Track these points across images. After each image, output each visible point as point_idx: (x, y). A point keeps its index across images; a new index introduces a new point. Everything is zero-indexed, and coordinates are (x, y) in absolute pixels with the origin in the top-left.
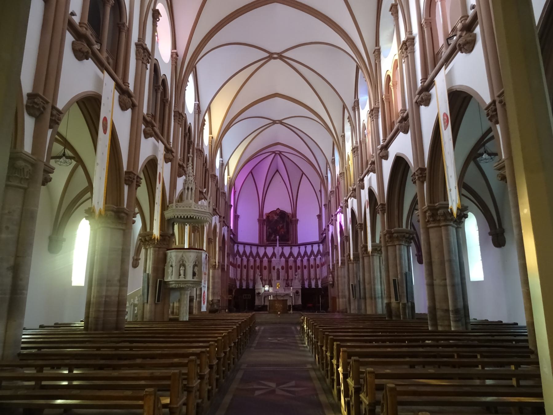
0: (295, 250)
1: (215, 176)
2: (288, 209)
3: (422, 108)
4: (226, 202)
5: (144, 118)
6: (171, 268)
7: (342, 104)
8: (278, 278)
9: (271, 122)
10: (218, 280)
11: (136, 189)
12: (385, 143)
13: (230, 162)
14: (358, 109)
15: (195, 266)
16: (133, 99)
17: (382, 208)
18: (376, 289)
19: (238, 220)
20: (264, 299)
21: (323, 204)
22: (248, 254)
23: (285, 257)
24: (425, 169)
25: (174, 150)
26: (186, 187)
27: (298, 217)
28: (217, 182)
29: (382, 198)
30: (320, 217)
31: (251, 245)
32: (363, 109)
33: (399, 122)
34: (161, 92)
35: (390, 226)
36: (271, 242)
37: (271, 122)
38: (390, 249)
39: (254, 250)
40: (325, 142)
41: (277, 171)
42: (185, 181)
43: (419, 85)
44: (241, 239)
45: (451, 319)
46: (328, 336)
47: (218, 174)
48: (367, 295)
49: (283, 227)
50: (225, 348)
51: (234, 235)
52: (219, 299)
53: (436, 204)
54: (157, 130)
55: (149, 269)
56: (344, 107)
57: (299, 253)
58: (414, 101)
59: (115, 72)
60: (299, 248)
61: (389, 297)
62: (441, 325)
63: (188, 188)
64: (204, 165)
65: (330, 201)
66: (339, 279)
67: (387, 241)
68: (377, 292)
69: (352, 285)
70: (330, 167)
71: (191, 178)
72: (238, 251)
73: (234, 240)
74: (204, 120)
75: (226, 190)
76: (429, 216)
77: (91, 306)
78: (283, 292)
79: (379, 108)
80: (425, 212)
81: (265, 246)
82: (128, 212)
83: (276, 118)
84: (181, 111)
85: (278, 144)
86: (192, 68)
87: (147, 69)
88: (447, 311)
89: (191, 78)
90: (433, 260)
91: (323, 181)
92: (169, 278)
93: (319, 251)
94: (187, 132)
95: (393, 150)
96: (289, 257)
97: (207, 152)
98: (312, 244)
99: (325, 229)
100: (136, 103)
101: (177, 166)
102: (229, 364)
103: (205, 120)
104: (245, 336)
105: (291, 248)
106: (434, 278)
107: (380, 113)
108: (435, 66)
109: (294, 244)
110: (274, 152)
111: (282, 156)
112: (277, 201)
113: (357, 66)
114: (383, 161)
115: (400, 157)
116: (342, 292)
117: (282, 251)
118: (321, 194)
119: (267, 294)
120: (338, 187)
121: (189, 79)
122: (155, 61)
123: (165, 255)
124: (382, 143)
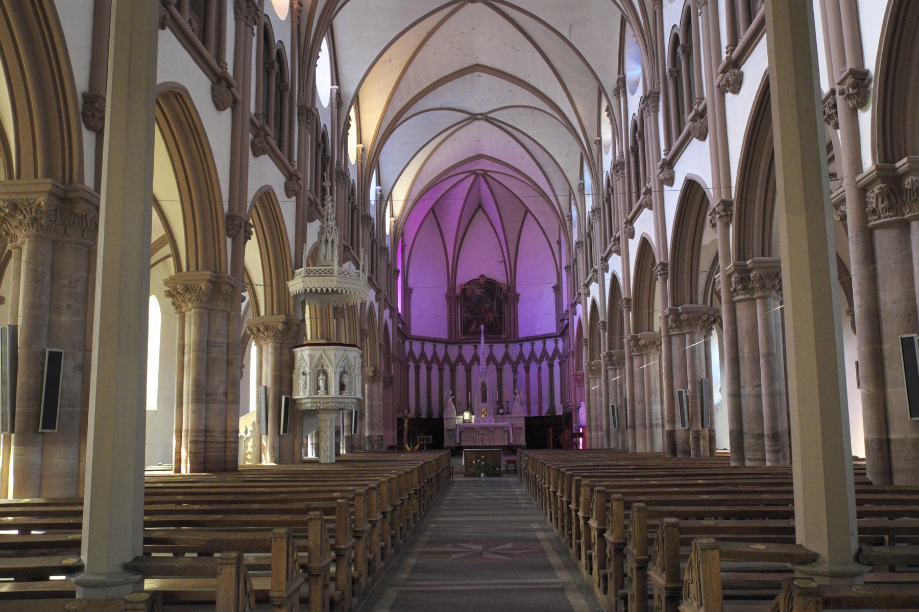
0: (514, 351)
1: (370, 218)
2: (498, 274)
3: (729, 96)
4: (388, 265)
5: (252, 122)
6: (303, 377)
7: (596, 85)
8: (484, 400)
9: (466, 116)
10: (378, 402)
11: (245, 243)
12: (668, 158)
13: (397, 195)
14: (625, 92)
15: (342, 374)
16: (234, 90)
17: (662, 270)
18: (654, 411)
19: (410, 296)
20: (460, 435)
21: (564, 265)
22: (429, 358)
23: (495, 362)
24: (731, 203)
25: (301, 176)
26: (323, 240)
27: (519, 290)
28: (373, 230)
29: (661, 254)
30: (557, 289)
31: (435, 341)
32: (633, 93)
33: (692, 120)
34: (277, 74)
35: (675, 303)
36: (471, 336)
37: (466, 116)
38: (676, 341)
39: (441, 350)
40: (566, 154)
41: (480, 206)
42: (322, 228)
43: (724, 56)
44: (414, 332)
45: (767, 448)
46: (564, 473)
47: (373, 213)
48: (638, 423)
49: (491, 309)
50: (401, 494)
51: (403, 324)
52: (381, 434)
53: (748, 262)
54: (274, 143)
55: (267, 379)
56: (601, 91)
57: (521, 355)
58: (716, 84)
59: (204, 44)
60: (521, 346)
61: (672, 421)
62: (750, 460)
63: (326, 241)
64: (349, 199)
65: (576, 260)
66: (592, 397)
67: (671, 328)
68: (654, 416)
69: (613, 406)
70: (575, 199)
71: (332, 224)
72: (411, 352)
73: (404, 333)
74: (349, 118)
75: (388, 243)
76: (736, 282)
77: (184, 434)
78: (494, 423)
79: (659, 93)
80: (730, 276)
81: (460, 343)
82: (233, 283)
83: (477, 110)
84: (309, 105)
85: (480, 157)
86: (327, 27)
87: (254, 35)
88: (761, 436)
89: (324, 45)
90: (741, 354)
91: (564, 223)
92: (301, 394)
93: (556, 350)
94: (321, 141)
95: (683, 170)
96: (503, 362)
97: (353, 176)
98: (544, 338)
99: (567, 311)
100: (239, 97)
101: (307, 203)
102: (408, 521)
103: (350, 119)
104: (431, 489)
105: (507, 346)
106: (742, 384)
107: (661, 104)
108: (751, 23)
109: (512, 339)
110: (473, 172)
111: (488, 178)
112: (481, 261)
113: (622, 17)
114: (666, 187)
115: (694, 181)
116: (597, 420)
117: (491, 352)
118: (560, 249)
119: (467, 428)
120: (589, 235)
121: (322, 48)
122: (264, 19)
123: (292, 357)
124: (663, 157)
